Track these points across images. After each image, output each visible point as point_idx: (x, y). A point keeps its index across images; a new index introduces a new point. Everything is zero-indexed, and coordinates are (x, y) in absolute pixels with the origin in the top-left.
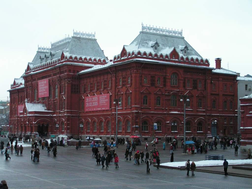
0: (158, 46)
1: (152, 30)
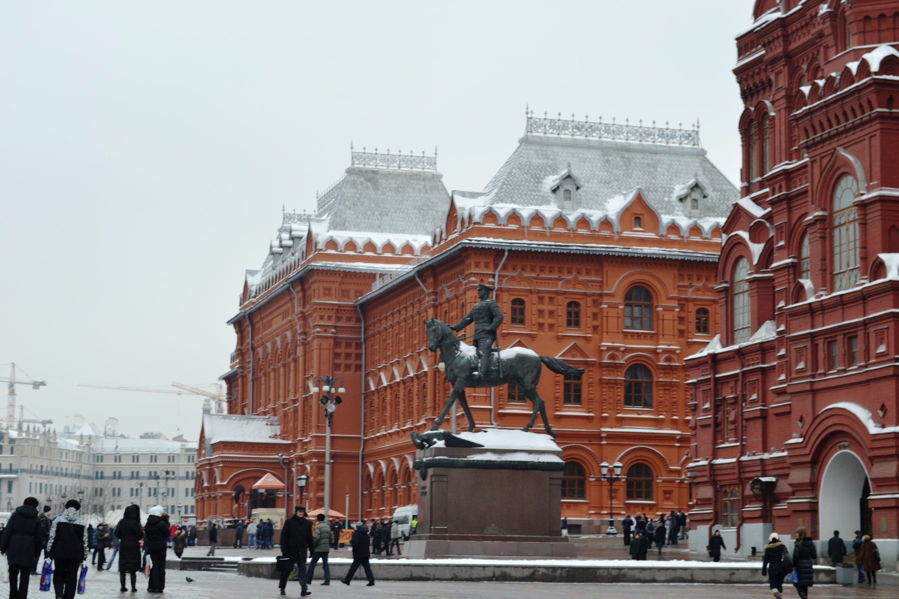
0: (578, 188)
1: (570, 130)
